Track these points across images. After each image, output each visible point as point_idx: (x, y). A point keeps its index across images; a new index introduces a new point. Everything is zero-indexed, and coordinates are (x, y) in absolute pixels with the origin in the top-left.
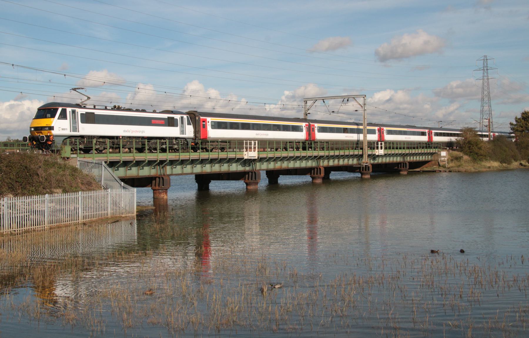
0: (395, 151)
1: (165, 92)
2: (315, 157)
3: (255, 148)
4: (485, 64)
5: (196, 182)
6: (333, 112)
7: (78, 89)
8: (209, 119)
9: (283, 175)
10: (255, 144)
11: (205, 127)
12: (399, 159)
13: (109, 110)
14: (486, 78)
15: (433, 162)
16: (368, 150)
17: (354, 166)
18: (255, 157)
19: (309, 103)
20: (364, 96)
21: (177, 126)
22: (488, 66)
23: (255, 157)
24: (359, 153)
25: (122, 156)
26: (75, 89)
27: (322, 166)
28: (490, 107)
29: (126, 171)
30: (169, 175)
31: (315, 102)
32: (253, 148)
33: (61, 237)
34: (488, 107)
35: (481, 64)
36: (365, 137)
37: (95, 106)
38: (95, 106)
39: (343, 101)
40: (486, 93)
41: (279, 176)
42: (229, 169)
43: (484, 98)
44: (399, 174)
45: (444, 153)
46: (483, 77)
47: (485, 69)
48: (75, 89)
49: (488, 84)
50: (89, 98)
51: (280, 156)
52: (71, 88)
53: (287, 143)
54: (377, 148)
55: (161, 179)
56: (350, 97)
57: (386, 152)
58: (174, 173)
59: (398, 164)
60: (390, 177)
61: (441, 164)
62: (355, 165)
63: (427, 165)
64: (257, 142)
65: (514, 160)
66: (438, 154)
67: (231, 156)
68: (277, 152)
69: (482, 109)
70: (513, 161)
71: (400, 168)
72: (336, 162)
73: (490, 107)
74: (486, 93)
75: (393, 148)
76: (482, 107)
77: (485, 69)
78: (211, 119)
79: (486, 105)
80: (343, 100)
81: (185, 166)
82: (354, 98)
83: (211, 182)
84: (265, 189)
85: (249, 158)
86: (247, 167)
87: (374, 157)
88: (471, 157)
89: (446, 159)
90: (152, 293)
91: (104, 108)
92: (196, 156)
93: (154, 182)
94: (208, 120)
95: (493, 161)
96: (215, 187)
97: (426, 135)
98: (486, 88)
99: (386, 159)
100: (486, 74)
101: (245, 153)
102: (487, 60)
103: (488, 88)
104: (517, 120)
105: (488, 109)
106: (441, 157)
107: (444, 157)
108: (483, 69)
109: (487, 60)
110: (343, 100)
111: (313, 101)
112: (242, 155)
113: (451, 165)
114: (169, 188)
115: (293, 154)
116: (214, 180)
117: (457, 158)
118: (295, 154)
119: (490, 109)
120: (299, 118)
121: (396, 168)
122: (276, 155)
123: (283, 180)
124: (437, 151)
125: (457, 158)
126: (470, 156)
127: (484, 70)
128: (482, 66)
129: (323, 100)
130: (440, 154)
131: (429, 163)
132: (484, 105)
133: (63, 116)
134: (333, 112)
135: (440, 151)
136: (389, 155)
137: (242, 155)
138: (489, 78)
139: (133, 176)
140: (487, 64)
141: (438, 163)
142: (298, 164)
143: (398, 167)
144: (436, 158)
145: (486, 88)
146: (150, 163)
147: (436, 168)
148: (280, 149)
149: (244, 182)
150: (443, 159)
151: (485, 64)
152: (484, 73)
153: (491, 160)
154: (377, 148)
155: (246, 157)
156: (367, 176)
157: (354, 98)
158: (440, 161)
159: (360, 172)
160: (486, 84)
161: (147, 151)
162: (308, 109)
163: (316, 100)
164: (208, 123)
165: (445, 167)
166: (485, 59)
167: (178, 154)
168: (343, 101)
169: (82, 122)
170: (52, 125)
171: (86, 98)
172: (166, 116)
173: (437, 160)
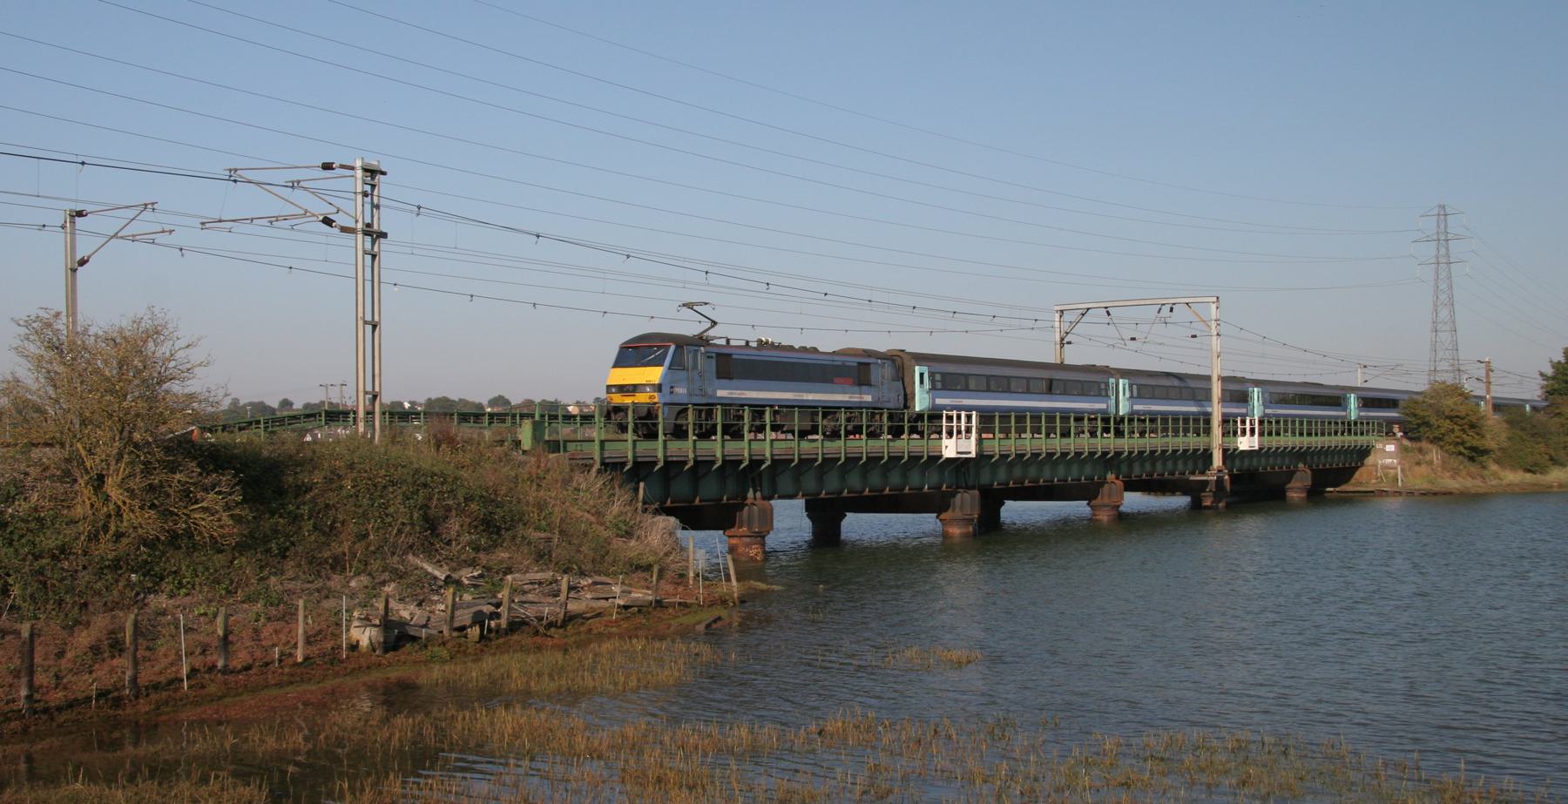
3: (968, 430)
5: (808, 515)
6: (1133, 339)
9: (1015, 499)
18: (970, 453)
23: (970, 453)
26: (690, 306)
31: (1083, 315)
32: (1248, 429)
37: (728, 341)
38: (728, 341)
39: (1159, 312)
40: (1443, 297)
43: (1439, 309)
47: (1443, 239)
48: (690, 306)
50: (714, 323)
52: (681, 303)
54: (1244, 433)
74: (1443, 297)
77: (1443, 239)
80: (1160, 309)
83: (1004, 503)
84: (807, 539)
87: (1230, 455)
90: (920, 745)
98: (1443, 286)
100: (1443, 251)
101: (946, 442)
102: (1446, 215)
108: (1435, 237)
109: (1446, 215)
110: (1160, 309)
114: (769, 533)
120: (1094, 366)
123: (1014, 511)
128: (1435, 231)
129: (1106, 308)
134: (1133, 339)
145: (1443, 286)
148: (1055, 434)
151: (1442, 226)
161: (692, 437)
162: (1067, 333)
168: (1159, 312)
171: (709, 324)
173: (1373, 466)
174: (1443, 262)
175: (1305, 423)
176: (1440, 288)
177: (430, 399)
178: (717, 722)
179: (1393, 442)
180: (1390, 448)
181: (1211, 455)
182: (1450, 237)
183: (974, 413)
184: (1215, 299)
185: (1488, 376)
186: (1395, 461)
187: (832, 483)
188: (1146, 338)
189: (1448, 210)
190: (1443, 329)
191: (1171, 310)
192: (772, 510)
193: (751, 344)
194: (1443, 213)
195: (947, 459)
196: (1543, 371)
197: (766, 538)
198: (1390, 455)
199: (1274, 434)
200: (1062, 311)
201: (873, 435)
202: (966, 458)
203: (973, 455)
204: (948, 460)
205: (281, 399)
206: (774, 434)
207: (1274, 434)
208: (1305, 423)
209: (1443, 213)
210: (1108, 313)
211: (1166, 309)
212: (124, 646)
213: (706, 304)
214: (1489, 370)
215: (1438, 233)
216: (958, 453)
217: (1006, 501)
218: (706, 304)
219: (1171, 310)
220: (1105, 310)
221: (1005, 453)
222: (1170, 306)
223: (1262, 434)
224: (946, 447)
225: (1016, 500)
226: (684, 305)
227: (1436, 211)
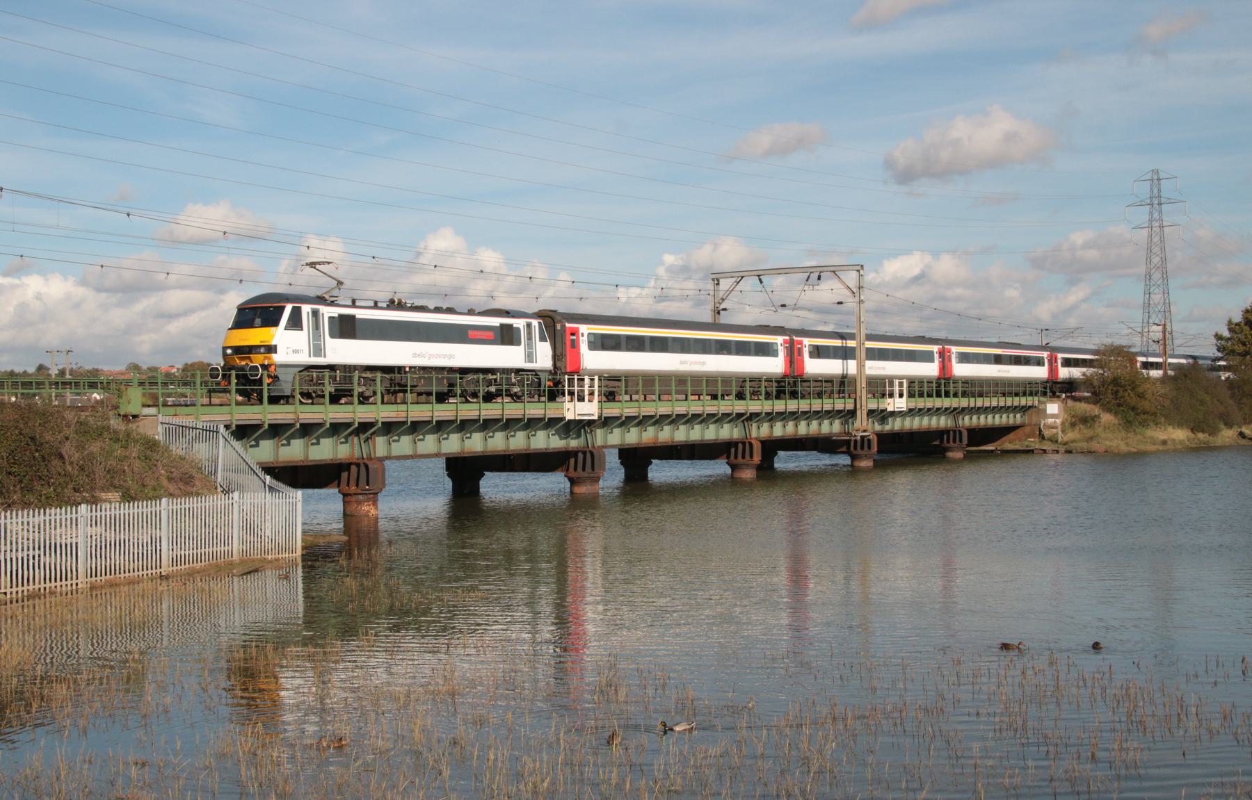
0: (934, 401)
2: (739, 415)
3: (592, 394)
4: (1156, 191)
5: (448, 475)
6: (783, 306)
8: (584, 329)
11: (575, 345)
12: (943, 422)
13: (382, 308)
15: (1027, 429)
16: (867, 398)
17: (834, 438)
19: (725, 284)
20: (858, 268)
21: (519, 344)
22: (1163, 194)
27: (757, 439)
28: (1166, 295)
29: (278, 448)
30: (381, 460)
33: (118, 608)
34: (1161, 295)
35: (1144, 190)
39: (807, 280)
40: (1156, 260)
41: (651, 463)
42: (529, 445)
44: (944, 457)
45: (1053, 408)
47: (1156, 202)
48: (312, 265)
49: (1162, 240)
53: (745, 381)
55: (363, 469)
56: (825, 269)
57: (912, 405)
58: (394, 453)
59: (941, 433)
61: (1047, 433)
62: (836, 435)
63: (1011, 436)
64: (596, 378)
65: (1226, 424)
66: (1039, 410)
67: (532, 412)
69: (1146, 301)
70: (1223, 426)
71: (945, 444)
73: (1166, 295)
74: (1156, 260)
77: (1156, 202)
78: (588, 329)
79: (1157, 291)
80: (809, 277)
81: (421, 437)
82: (834, 272)
86: (572, 439)
88: (1120, 416)
89: (1058, 421)
91: (372, 304)
92: (448, 413)
93: (345, 475)
94: (581, 331)
95: (1174, 428)
96: (494, 487)
98: (1156, 250)
100: (1156, 215)
101: (568, 405)
102: (1159, 179)
103: (1163, 249)
104: (1232, 327)
105: (1162, 301)
106: (1046, 416)
107: (1053, 416)
109: (1159, 179)
110: (809, 277)
111: (734, 279)
112: (560, 412)
113: (1071, 435)
115: (684, 409)
116: (491, 470)
117: (1086, 420)
119: (1167, 301)
121: (937, 443)
124: (1036, 403)
125: (1086, 420)
126: (1116, 414)
127: (1152, 205)
128: (1149, 196)
129: (759, 276)
130: (1045, 410)
131: (1017, 431)
133: (295, 322)
134: (783, 306)
135: (1044, 403)
137: (560, 412)
138: (1165, 224)
139: (289, 462)
140: (1159, 190)
141: (1040, 431)
142: (696, 434)
143: (942, 441)
144: (1034, 419)
146: (336, 429)
147: (1033, 443)
149: (566, 476)
150: (1050, 421)
151: (1156, 191)
152: (1151, 213)
153: (1169, 425)
155: (569, 416)
156: (865, 463)
157: (834, 272)
158: (1044, 425)
159: (848, 453)
160: (1156, 239)
162: (723, 300)
163: (742, 277)
164: (581, 338)
165: (1057, 441)
166: (1156, 177)
167: (520, 405)
168: (807, 280)
169: (332, 336)
170: (273, 343)
172: (496, 321)
176: (1154, 251)
177: (187, 364)
178: (40, 589)
182: (1163, 200)
189: (1162, 175)
191: (819, 278)
192: (384, 470)
193: (380, 305)
196: (1219, 333)
197: (342, 496)
199: (960, 394)
201: (364, 400)
202: (589, 420)
205: (184, 363)
207: (960, 394)
210: (761, 281)
213: (329, 263)
218: (329, 263)
221: (335, 421)
222: (818, 274)
226: (307, 264)
227: (1149, 176)
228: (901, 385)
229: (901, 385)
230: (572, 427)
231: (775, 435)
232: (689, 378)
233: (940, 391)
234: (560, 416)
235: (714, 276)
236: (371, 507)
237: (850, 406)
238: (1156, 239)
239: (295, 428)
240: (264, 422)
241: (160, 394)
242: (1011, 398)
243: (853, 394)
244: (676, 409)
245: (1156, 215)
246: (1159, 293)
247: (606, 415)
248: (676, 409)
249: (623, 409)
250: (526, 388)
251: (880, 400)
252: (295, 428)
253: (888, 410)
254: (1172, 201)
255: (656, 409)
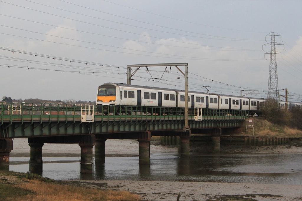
1: (12, 51)
4: (273, 40)
5: (29, 144)
6: (156, 79)
7: (207, 86)
10: (91, 108)
14: (274, 52)
18: (92, 120)
20: (186, 65)
23: (92, 120)
24: (170, 118)
25: (137, 117)
26: (206, 87)
28: (277, 79)
34: (275, 79)
35: (269, 39)
36: (156, 114)
39: (166, 69)
41: (106, 140)
43: (271, 70)
46: (271, 51)
47: (273, 44)
48: (206, 87)
49: (275, 58)
51: (113, 120)
56: (173, 65)
57: (99, 119)
60: (59, 154)
68: (162, 116)
69: (270, 81)
72: (116, 129)
73: (277, 79)
74: (273, 66)
75: (210, 115)
76: (270, 79)
77: (273, 44)
79: (273, 77)
80: (166, 67)
82: (176, 66)
83: (44, 144)
85: (198, 120)
87: (192, 122)
97: (174, 100)
98: (273, 62)
99: (135, 128)
100: (273, 49)
102: (274, 36)
103: (276, 62)
105: (275, 81)
108: (271, 44)
109: (274, 36)
110: (166, 67)
111: (137, 68)
112: (79, 119)
118: (126, 118)
119: (277, 81)
122: (110, 119)
127: (272, 45)
132: (271, 77)
134: (156, 79)
136: (107, 123)
138: (276, 52)
140: (274, 40)
151: (273, 40)
154: (196, 114)
155: (196, 120)
157: (176, 66)
158: (247, 127)
160: (273, 58)
163: (140, 67)
166: (273, 35)
168: (166, 69)
174: (283, 96)
175: (86, 108)
179: (252, 118)
180: (250, 121)
181: (184, 122)
182: (276, 44)
183: (93, 105)
184: (186, 65)
185: (286, 95)
186: (252, 125)
187: (37, 133)
188: (161, 78)
190: (273, 77)
191: (171, 68)
194: (273, 36)
195: (83, 122)
198: (251, 123)
200: (130, 67)
203: (201, 120)
204: (196, 121)
206: (122, 114)
208: (86, 108)
209: (273, 36)
211: (169, 67)
212: (251, 138)
214: (287, 93)
215: (272, 42)
216: (87, 120)
217: (107, 139)
219: (171, 68)
220: (146, 67)
221: (5, 122)
223: (203, 114)
224: (83, 118)
225: (111, 139)
227: (271, 34)
228: (200, 110)
229: (200, 110)
230: (83, 126)
231: (126, 131)
232: (201, 109)
233: (233, 112)
234: (79, 121)
235: (129, 66)
236: (7, 158)
237: (182, 118)
238: (273, 58)
239: (11, 124)
240: (2, 122)
241: (205, 113)
242: (238, 117)
243: (183, 113)
244: (104, 119)
245: (273, 49)
246: (274, 78)
247: (96, 121)
248: (104, 119)
249: (126, 118)
250: (220, 112)
251: (193, 116)
252: (11, 124)
253: (195, 120)
254: (279, 44)
255: (114, 118)
